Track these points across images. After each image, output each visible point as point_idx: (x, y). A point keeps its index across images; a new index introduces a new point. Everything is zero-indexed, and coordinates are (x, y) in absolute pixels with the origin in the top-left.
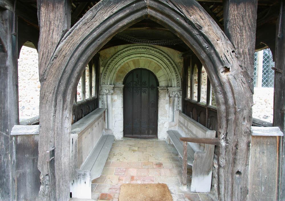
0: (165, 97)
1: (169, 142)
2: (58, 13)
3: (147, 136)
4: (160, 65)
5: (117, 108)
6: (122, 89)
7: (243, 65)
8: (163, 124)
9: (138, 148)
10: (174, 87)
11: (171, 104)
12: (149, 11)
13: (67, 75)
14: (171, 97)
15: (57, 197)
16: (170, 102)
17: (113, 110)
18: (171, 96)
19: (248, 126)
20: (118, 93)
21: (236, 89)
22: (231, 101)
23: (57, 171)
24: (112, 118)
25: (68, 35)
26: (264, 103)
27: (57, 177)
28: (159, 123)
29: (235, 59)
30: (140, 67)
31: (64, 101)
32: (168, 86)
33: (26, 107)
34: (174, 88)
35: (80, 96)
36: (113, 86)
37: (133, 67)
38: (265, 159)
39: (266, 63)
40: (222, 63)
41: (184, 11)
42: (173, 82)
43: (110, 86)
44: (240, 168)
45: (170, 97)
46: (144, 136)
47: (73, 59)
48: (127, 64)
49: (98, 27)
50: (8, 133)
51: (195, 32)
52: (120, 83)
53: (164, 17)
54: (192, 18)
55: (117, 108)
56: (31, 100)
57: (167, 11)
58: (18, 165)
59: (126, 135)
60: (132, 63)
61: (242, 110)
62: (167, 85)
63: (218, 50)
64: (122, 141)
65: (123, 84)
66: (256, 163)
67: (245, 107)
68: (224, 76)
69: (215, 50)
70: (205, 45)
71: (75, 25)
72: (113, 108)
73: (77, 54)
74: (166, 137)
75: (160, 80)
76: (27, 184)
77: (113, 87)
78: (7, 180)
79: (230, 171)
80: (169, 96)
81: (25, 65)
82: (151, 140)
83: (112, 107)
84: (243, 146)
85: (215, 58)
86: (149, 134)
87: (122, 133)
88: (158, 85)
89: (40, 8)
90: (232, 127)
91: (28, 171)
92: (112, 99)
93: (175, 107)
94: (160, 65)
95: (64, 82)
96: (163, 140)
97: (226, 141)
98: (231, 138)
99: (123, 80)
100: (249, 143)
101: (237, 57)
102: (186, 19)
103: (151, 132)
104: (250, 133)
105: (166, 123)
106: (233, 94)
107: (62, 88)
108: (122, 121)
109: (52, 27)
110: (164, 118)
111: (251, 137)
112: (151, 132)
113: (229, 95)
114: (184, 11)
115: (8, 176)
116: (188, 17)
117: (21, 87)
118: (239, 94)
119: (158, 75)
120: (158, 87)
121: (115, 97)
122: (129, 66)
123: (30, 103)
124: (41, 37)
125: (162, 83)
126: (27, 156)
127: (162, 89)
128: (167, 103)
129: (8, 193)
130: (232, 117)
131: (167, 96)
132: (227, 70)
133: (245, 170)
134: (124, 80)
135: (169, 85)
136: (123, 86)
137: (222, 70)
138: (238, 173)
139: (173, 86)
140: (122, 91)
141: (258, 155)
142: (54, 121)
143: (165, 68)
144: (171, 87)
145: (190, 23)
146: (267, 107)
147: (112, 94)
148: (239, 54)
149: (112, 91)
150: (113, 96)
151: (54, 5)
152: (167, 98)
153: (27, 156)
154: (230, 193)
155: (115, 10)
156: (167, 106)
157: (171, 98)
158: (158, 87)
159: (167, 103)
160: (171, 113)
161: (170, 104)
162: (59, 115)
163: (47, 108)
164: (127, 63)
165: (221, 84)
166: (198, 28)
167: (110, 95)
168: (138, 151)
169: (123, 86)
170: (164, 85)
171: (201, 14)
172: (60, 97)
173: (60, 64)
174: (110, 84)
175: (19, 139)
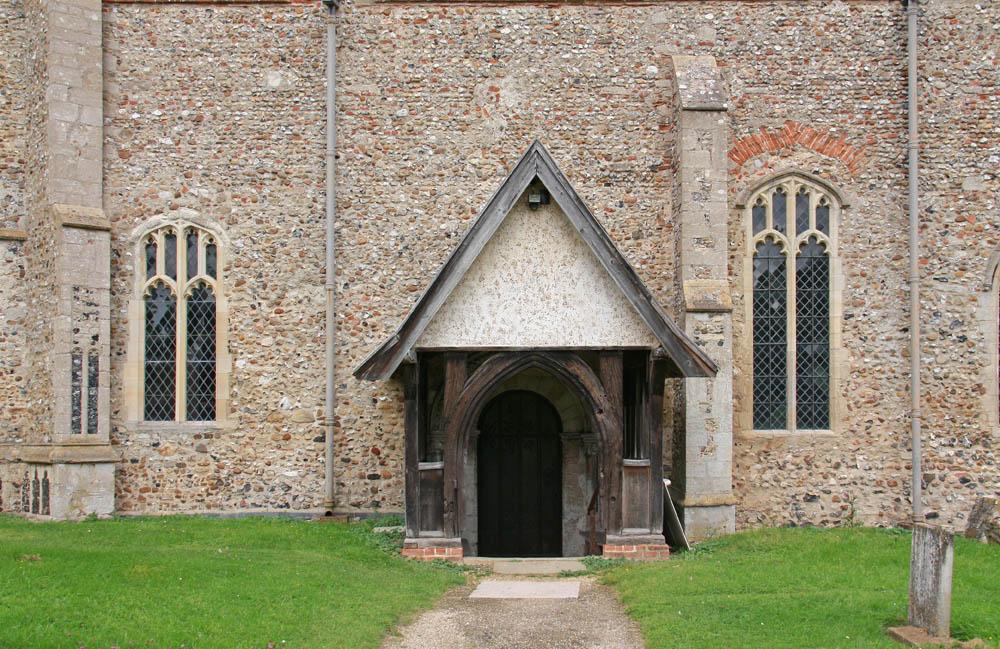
0: (577, 457)
18: (589, 452)
23: (459, 497)
26: (804, 465)
33: (253, 486)
35: (380, 458)
38: (638, 487)
40: (598, 406)
44: (614, 494)
45: (587, 456)
54: (570, 369)
58: (422, 497)
75: (564, 416)
88: (560, 430)
98: (606, 469)
105: (581, 520)
117: (847, 409)
119: (559, 405)
128: (582, 473)
131: (581, 454)
132: (601, 412)
135: (586, 430)
136: (479, 432)
138: (613, 498)
141: (632, 485)
151: (458, 362)
152: (582, 460)
153: (430, 490)
155: (507, 365)
157: (590, 460)
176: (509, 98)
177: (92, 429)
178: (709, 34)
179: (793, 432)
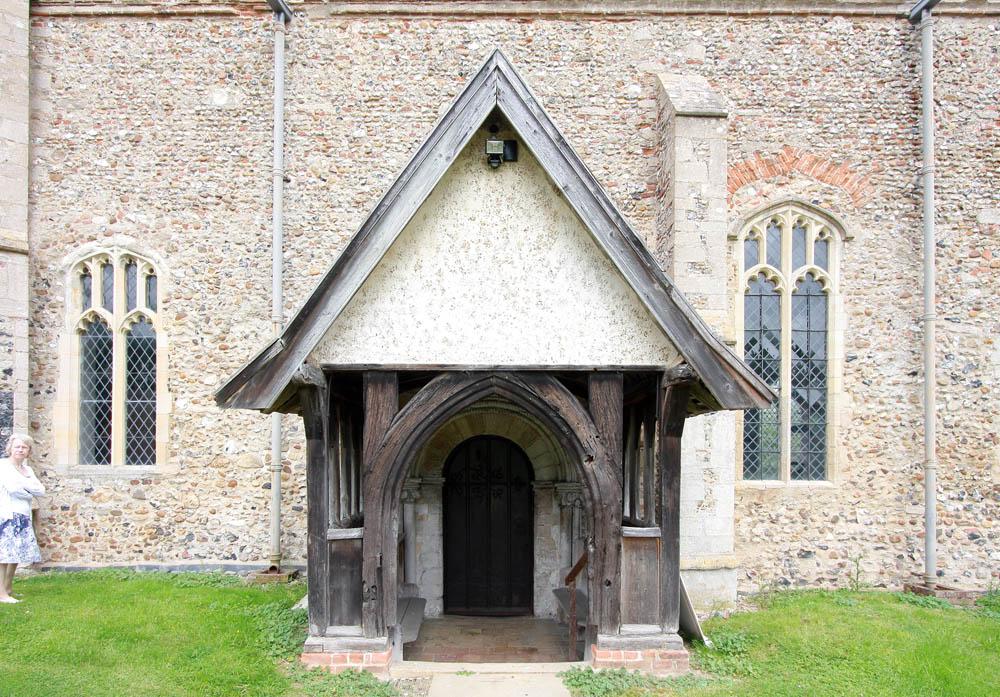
1: (562, 619)
2: (388, 395)
3: (506, 610)
4: (536, 427)
5: (428, 537)
6: (440, 488)
7: (609, 453)
8: (547, 576)
9: (483, 630)
10: (571, 482)
11: (565, 526)
12: (495, 389)
13: (397, 467)
14: (564, 507)
15: (385, 615)
16: (562, 518)
17: (418, 541)
18: (564, 504)
19: (617, 525)
20: (431, 498)
21: (602, 481)
22: (596, 496)
24: (416, 561)
25: (401, 416)
27: (385, 590)
28: (536, 575)
29: (600, 445)
30: (485, 434)
31: (393, 497)
32: (556, 481)
34: (570, 485)
36: (419, 481)
37: (467, 434)
39: (753, 425)
41: (537, 390)
42: (567, 471)
43: (412, 480)
44: (609, 576)
45: (561, 507)
46: (499, 609)
47: (405, 447)
48: (452, 427)
49: (435, 410)
50: (323, 538)
51: (552, 414)
52: (435, 472)
53: (515, 396)
54: (546, 399)
55: (428, 537)
56: (211, 517)
57: (518, 390)
59: (450, 609)
60: (464, 422)
61: (609, 506)
62: (553, 477)
63: (579, 435)
64: (441, 620)
65: (443, 476)
66: (632, 574)
67: (612, 502)
68: (586, 465)
69: (576, 436)
70: (565, 429)
71: (407, 406)
72: (418, 537)
73: (410, 441)
74: (554, 611)
76: (343, 603)
77: (420, 484)
78: (321, 597)
79: (598, 581)
80: (560, 505)
81: (199, 431)
82: (515, 619)
83: (416, 534)
84: (612, 549)
85: (578, 445)
86: (509, 604)
87: (441, 602)
89: (367, 389)
90: (599, 529)
91: (344, 586)
92: (415, 514)
93: (575, 532)
94: (536, 427)
95: (394, 474)
96: (546, 617)
97: (594, 546)
98: (598, 540)
99: (442, 466)
100: (619, 547)
101: (602, 443)
102: (540, 399)
103: (516, 599)
104: (619, 534)
105: (554, 575)
106: (598, 487)
107: (392, 481)
108: (441, 571)
109: (380, 411)
110: (549, 561)
111: (621, 539)
112: (516, 599)
113: (594, 488)
114: (537, 390)
115: (322, 591)
116: (542, 396)
118: (605, 487)
119: (530, 452)
120: (532, 483)
121: (424, 510)
122: (458, 431)
123: (209, 524)
124: (367, 421)
125: (543, 473)
126: (344, 567)
127: (542, 489)
129: (322, 613)
130: (599, 515)
131: (555, 504)
132: (591, 459)
133: (616, 580)
134: (446, 464)
135: (560, 478)
136: (443, 480)
137: (585, 459)
138: (609, 583)
139: (568, 479)
140: (441, 493)
142: (382, 522)
143: (548, 436)
144: (564, 481)
145: (545, 403)
146: (806, 529)
147: (416, 501)
148: (604, 439)
149: (417, 494)
150: (418, 506)
152: (556, 510)
154: (599, 608)
155: (456, 391)
156: (555, 530)
157: (565, 510)
158: (532, 483)
159: (555, 524)
160: (565, 547)
161: (562, 524)
162: (387, 515)
163: (374, 506)
164: (454, 423)
165: (586, 476)
166: (556, 410)
167: (411, 503)
168: (483, 634)
169: (443, 480)
170: (546, 477)
171: (558, 394)
172: (389, 493)
173: (390, 455)
174: (413, 477)
175: (334, 546)
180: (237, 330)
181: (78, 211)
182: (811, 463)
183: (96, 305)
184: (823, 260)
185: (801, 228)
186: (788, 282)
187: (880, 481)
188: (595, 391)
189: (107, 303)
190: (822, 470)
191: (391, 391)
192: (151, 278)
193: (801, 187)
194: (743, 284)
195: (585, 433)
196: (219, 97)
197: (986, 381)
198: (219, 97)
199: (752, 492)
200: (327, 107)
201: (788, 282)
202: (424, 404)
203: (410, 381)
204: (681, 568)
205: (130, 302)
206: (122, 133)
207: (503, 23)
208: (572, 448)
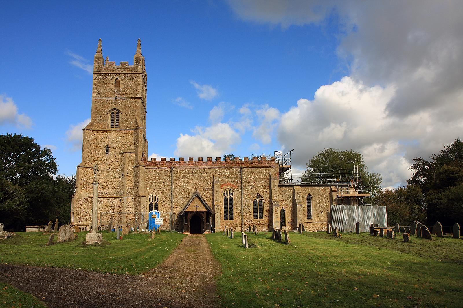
42: (118, 254)
176: (194, 180)
177: (261, 217)
178: (218, 172)
179: (258, 220)
180: (167, 204)
181: (149, 191)
182: (232, 218)
183: (151, 201)
184: (232, 195)
185: (230, 192)
186: (228, 198)
187: (239, 220)
188: (204, 213)
189: (152, 201)
190: (233, 218)
191: (189, 214)
192: (157, 198)
193: (229, 187)
194: (223, 198)
195: (203, 216)
196: (165, 177)
197: (250, 208)
198: (165, 177)
199: (225, 221)
200: (177, 179)
201: (228, 198)
202: (192, 214)
203: (190, 212)
204: (196, 211)
205: (155, 201)
206: (154, 182)
207: (197, 169)
208: (203, 217)
